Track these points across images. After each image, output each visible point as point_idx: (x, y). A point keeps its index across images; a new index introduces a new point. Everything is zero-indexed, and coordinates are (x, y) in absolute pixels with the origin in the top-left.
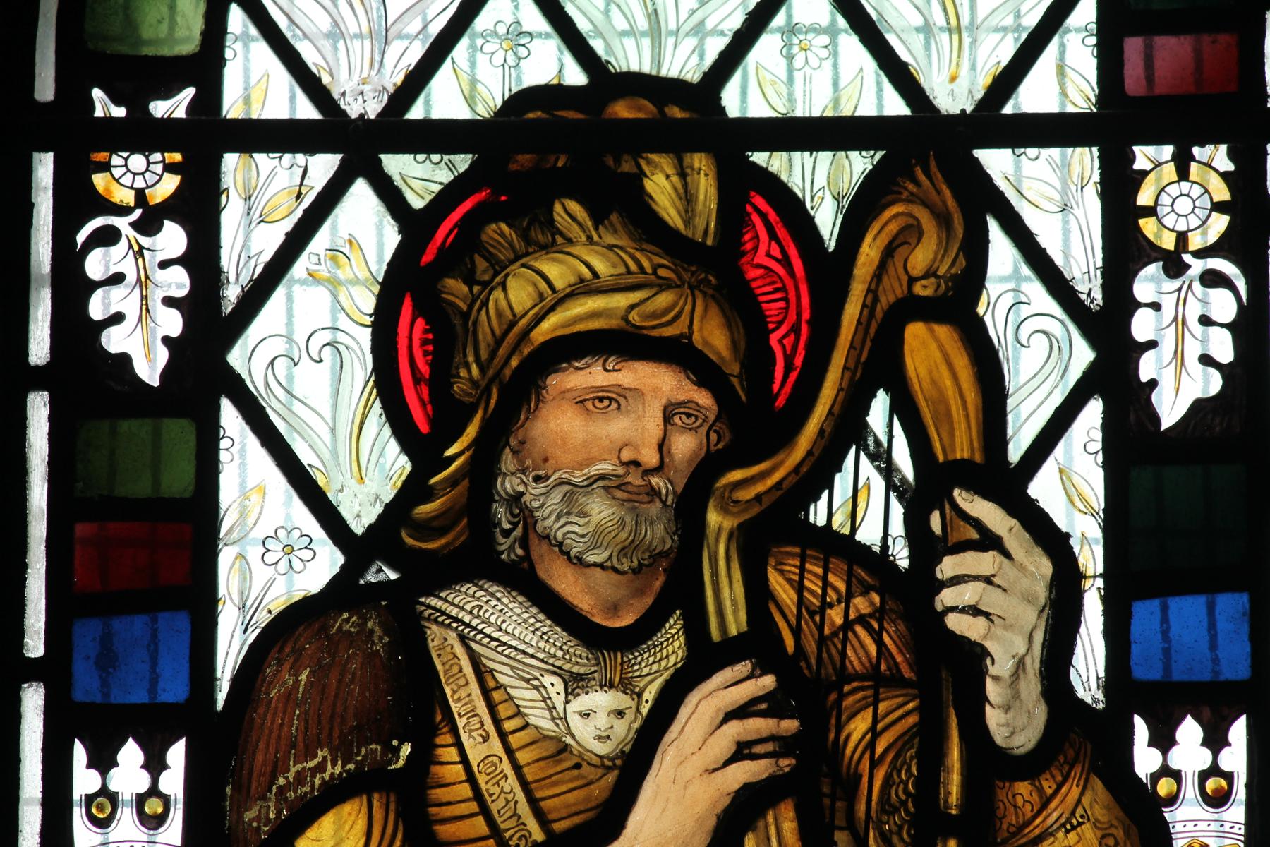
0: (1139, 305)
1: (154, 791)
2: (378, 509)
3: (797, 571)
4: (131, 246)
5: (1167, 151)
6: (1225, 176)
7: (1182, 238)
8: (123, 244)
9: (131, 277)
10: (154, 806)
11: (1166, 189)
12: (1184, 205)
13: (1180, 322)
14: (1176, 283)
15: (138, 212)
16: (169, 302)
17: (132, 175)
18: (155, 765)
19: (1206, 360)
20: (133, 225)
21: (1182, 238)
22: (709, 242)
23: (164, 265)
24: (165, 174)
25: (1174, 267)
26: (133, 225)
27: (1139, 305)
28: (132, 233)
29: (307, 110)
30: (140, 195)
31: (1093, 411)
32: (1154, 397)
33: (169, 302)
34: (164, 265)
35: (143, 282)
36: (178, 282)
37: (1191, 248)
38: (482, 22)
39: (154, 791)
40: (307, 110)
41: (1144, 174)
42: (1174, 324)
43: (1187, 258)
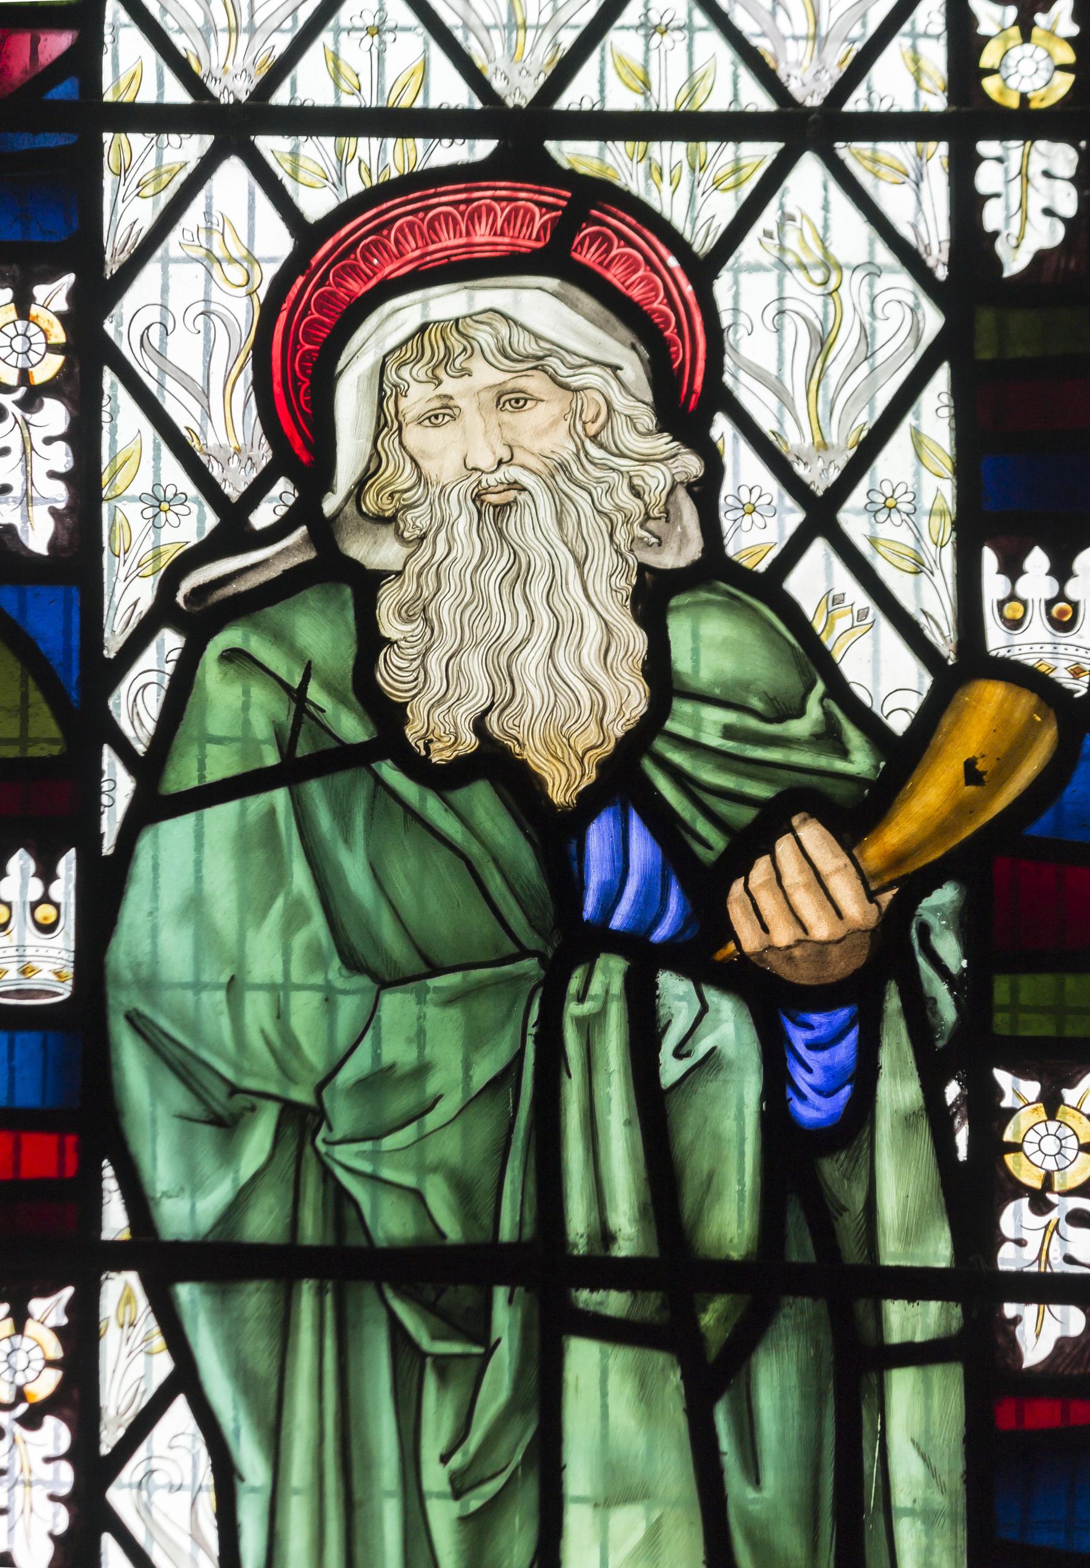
0: (1004, 1240)
1: (46, 899)
2: (246, 486)
3: (660, 745)
4: (16, 421)
5: (1012, 12)
6: (1070, 40)
7: (1048, 1178)
8: (10, 420)
9: (17, 492)
10: (45, 913)
11: (1035, 1128)
12: (1027, 67)
13: (1024, 175)
14: (1043, 1220)
15: (22, 390)
16: (53, 475)
17: (12, 336)
18: (47, 874)
19: (1048, 212)
20: (16, 403)
21: (1048, 1178)
22: (568, 194)
23: (48, 441)
24: (47, 354)
25: (1040, 1204)
26: (16, 403)
27: (1004, 1240)
28: (18, 412)
29: (177, 94)
30: (24, 375)
31: (942, 378)
32: (1018, 1330)
33: (53, 475)
34: (48, 441)
35: (27, 450)
36: (61, 457)
37: (1056, 1188)
38: (344, 15)
39: (46, 899)
40: (177, 94)
41: (987, 39)
42: (1037, 1262)
43: (1052, 1197)
